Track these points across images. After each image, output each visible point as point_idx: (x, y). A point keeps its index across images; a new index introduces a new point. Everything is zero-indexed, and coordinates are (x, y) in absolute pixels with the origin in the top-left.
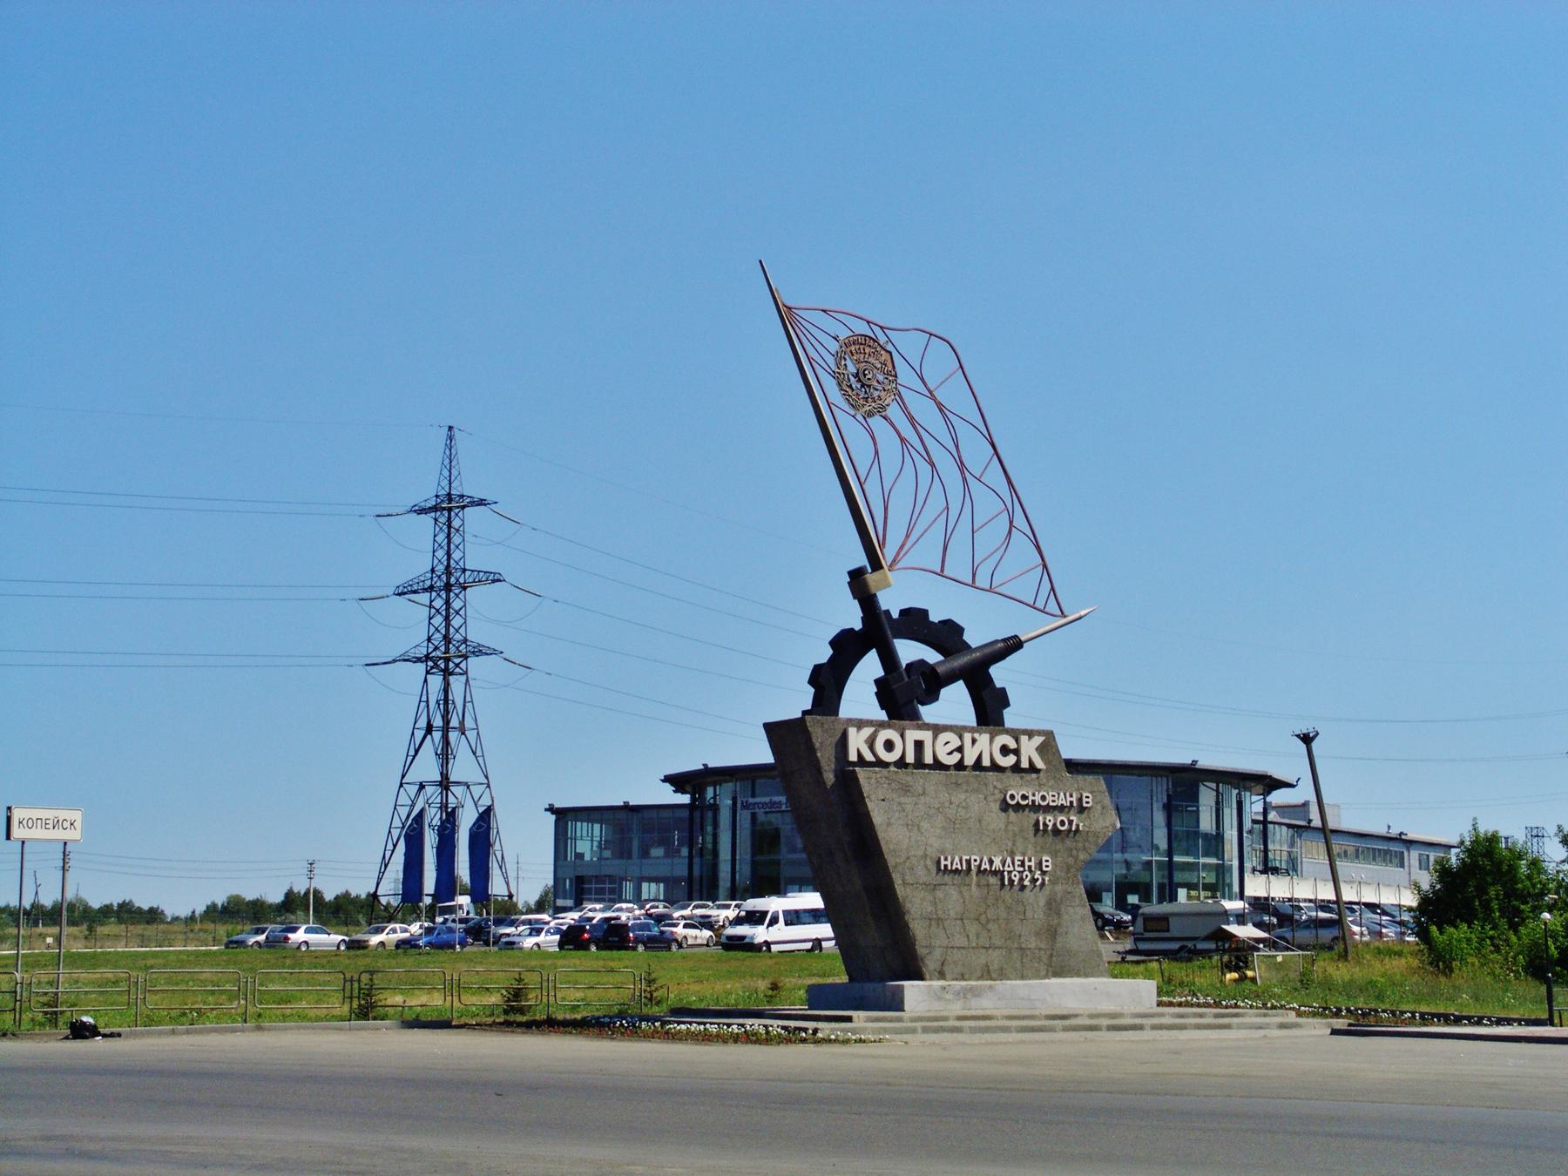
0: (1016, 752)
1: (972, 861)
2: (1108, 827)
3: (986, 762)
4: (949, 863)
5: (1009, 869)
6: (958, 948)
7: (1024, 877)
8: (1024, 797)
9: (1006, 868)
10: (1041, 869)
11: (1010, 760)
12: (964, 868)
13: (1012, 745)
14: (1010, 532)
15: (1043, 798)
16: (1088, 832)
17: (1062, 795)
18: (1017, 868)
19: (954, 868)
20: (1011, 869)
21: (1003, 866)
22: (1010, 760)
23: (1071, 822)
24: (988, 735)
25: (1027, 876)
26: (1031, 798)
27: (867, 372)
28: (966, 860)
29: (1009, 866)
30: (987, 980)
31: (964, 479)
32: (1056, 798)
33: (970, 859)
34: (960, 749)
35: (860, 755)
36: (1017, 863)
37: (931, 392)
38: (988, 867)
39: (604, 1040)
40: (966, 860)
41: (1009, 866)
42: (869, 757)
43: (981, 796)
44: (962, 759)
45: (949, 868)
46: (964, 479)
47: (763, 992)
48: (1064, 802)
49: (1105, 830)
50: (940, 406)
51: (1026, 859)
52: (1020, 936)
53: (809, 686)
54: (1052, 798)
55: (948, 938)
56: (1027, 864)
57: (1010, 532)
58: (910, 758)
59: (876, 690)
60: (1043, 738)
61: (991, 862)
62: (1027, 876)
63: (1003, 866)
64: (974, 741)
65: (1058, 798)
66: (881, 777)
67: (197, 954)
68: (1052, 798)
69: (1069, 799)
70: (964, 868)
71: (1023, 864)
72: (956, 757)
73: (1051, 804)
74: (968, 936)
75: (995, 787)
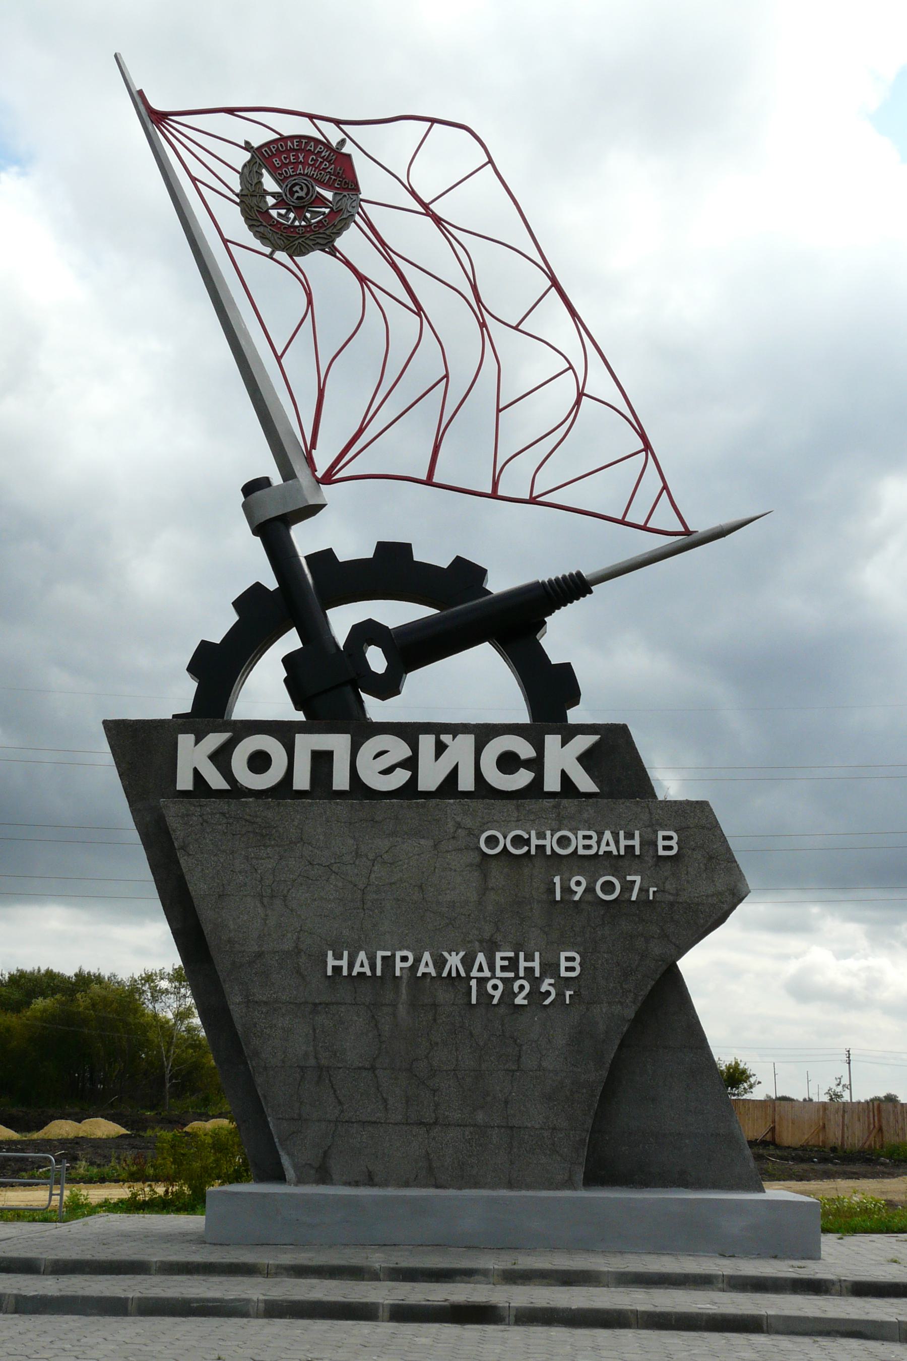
0: (537, 764)
1: (398, 959)
2: (720, 894)
3: (466, 783)
4: (344, 963)
5: (480, 975)
6: (363, 1123)
7: (516, 990)
8: (518, 841)
9: (474, 973)
10: (556, 974)
11: (522, 778)
12: (379, 973)
13: (525, 750)
14: (578, 403)
15: (563, 842)
16: (672, 904)
17: (608, 835)
18: (499, 973)
19: (354, 973)
20: (487, 973)
21: (468, 969)
22: (522, 778)
23: (628, 887)
24: (451, 736)
25: (522, 987)
26: (535, 842)
27: (297, 188)
28: (383, 958)
29: (481, 969)
30: (426, 1186)
31: (483, 325)
32: (593, 842)
33: (394, 955)
34: (411, 763)
35: (197, 776)
36: (499, 963)
37: (425, 206)
38: (431, 970)
39: (537, 1287)
40: (383, 958)
41: (481, 969)
42: (216, 781)
43: (426, 843)
44: (414, 779)
45: (345, 972)
46: (483, 325)
47: (65, 1203)
48: (613, 848)
49: (715, 900)
50: (438, 220)
51: (522, 955)
52: (506, 1102)
53: (577, 761)
54: (582, 842)
55: (340, 1103)
56: (522, 964)
57: (578, 403)
58: (302, 780)
59: (285, 674)
60: (227, 787)
61: (440, 963)
62: (522, 987)
63: (468, 969)
64: (440, 748)
65: (599, 843)
66: (212, 814)
67: (22, 1151)
68: (582, 842)
69: (623, 843)
70: (379, 973)
71: (513, 964)
72: (401, 777)
73: (581, 852)
74: (385, 1101)
75: (459, 826)
